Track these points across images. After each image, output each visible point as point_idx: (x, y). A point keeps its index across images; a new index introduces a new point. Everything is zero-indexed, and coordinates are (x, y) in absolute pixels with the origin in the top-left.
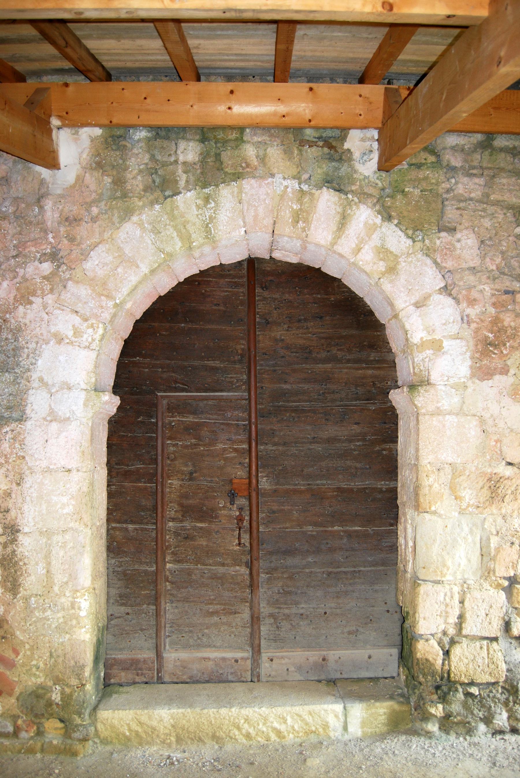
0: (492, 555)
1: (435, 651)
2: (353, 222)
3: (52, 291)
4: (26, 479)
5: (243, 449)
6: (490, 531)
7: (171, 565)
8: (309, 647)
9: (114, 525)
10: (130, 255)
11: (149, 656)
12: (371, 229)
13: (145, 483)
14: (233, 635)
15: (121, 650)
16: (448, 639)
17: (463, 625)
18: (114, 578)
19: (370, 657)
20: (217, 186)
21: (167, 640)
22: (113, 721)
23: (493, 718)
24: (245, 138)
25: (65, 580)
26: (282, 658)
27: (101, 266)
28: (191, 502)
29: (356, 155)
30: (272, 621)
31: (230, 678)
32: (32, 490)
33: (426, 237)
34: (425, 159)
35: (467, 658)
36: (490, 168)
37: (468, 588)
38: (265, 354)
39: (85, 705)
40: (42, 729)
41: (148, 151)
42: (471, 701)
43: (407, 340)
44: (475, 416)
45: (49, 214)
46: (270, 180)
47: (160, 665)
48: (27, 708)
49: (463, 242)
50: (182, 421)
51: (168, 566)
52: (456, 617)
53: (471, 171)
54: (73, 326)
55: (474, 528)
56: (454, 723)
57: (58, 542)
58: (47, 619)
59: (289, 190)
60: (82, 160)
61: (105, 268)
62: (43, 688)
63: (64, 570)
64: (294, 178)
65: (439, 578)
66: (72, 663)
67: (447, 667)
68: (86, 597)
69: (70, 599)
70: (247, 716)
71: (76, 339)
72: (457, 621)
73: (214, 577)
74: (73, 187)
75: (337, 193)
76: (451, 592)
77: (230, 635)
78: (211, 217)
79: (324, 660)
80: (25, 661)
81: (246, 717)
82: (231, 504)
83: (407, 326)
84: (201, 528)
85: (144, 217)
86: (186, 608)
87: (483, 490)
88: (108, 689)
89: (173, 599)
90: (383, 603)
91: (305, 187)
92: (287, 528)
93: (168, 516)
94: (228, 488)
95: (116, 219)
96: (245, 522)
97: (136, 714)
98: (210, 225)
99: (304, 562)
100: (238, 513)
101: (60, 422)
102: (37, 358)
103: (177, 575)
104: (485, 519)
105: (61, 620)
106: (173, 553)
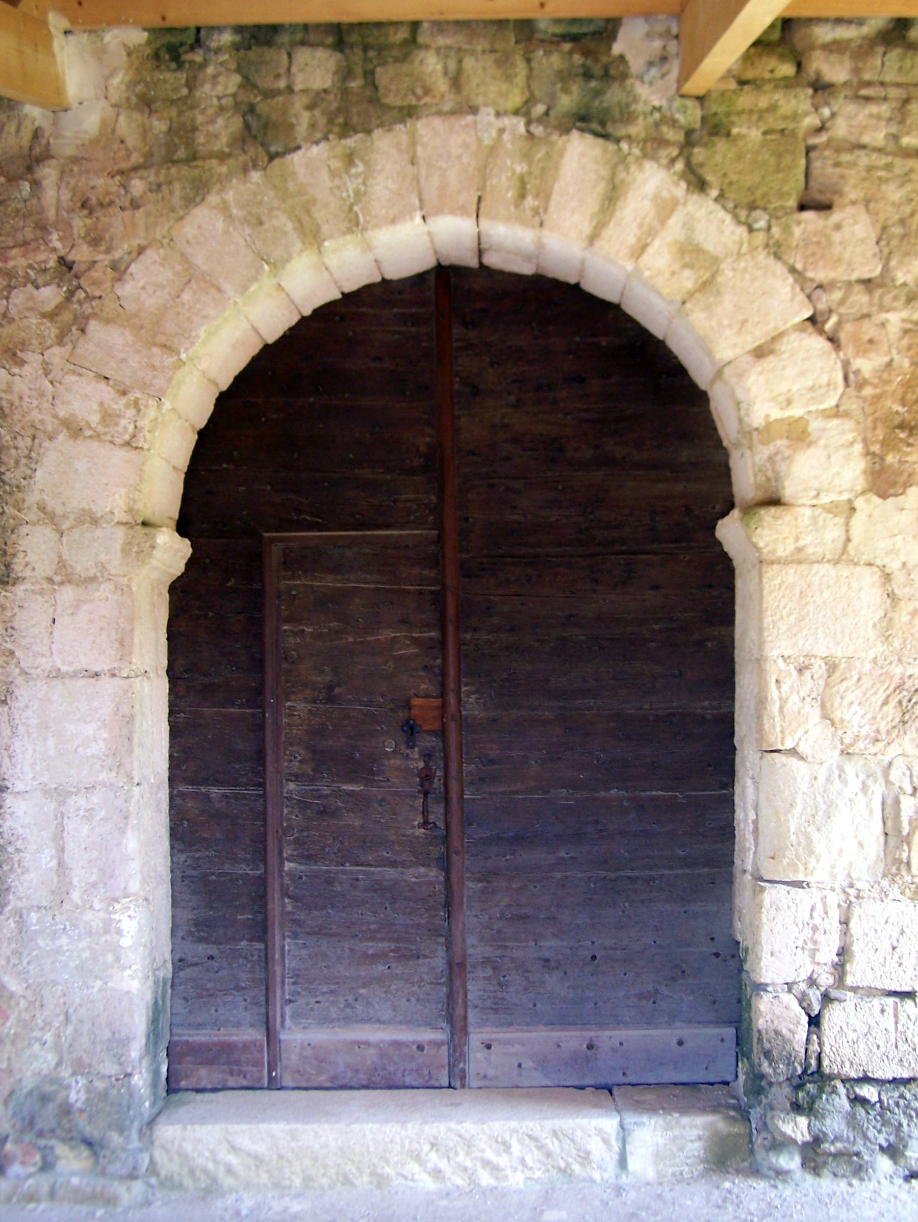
0: (905, 833)
1: (792, 1015)
2: (630, 195)
3: (60, 340)
4: (17, 693)
5: (431, 639)
6: (900, 787)
7: (292, 865)
8: (563, 1021)
9: (182, 788)
10: (205, 268)
11: (253, 1038)
12: (665, 209)
13: (240, 706)
14: (413, 1000)
15: (200, 1026)
16: (818, 993)
17: (848, 967)
18: (185, 889)
19: (680, 1043)
20: (369, 132)
21: (288, 1009)
22: (184, 1144)
23: (905, 1146)
24: (421, 40)
25: (93, 878)
26: (509, 1042)
27: (150, 289)
28: (330, 743)
29: (636, 64)
30: (489, 972)
31: (408, 1080)
32: (29, 713)
33: (773, 222)
34: (772, 71)
35: (855, 1031)
36: (898, 85)
37: (858, 897)
38: (472, 453)
39: (131, 1113)
40: (49, 1159)
41: (239, 70)
42: (863, 1112)
43: (740, 420)
44: (870, 564)
45: (50, 195)
46: (470, 118)
47: (275, 1056)
48: (23, 1119)
49: (846, 229)
50: (312, 586)
51: (288, 866)
52: (835, 951)
53: (864, 92)
54: (101, 404)
55: (869, 782)
56: (830, 1154)
57: (79, 809)
58: (59, 951)
59: (506, 136)
60: (111, 89)
61: (159, 293)
62: (53, 1081)
63: (90, 861)
64: (516, 113)
65: (800, 877)
66: (107, 1034)
67: (815, 1047)
68: (131, 913)
69: (102, 914)
70: (436, 1138)
71: (106, 430)
72: (836, 959)
73: (378, 888)
74: (95, 142)
75: (600, 141)
76: (824, 904)
77: (408, 1000)
78: (357, 192)
79: (590, 1047)
80: (19, 1030)
81: (432, 1139)
82: (409, 747)
83: (740, 394)
84: (351, 794)
85: (230, 196)
86: (324, 948)
87: (885, 708)
88: (175, 1097)
89: (299, 930)
90: (708, 939)
91: (538, 130)
92: (517, 792)
93: (287, 771)
94: (402, 715)
95: (176, 200)
96: (436, 780)
97: (227, 1132)
98: (356, 208)
99: (552, 859)
100: (421, 765)
101: (78, 586)
102: (33, 466)
103: (305, 883)
104: (890, 764)
105: (86, 954)
106: (296, 841)
